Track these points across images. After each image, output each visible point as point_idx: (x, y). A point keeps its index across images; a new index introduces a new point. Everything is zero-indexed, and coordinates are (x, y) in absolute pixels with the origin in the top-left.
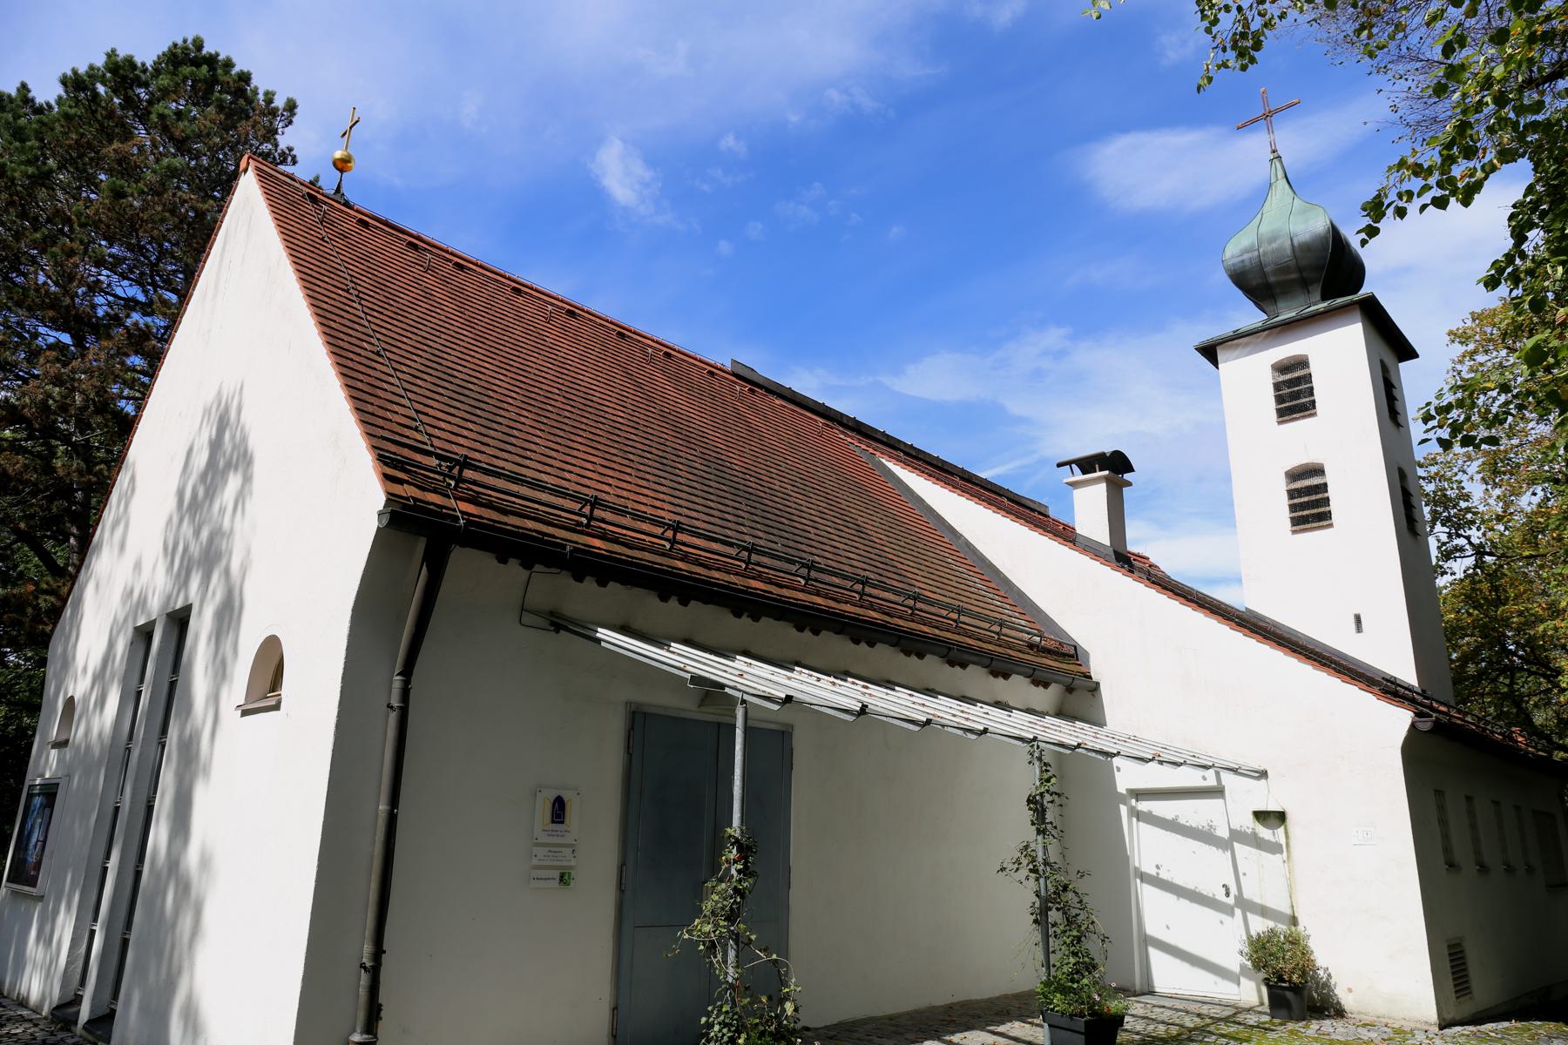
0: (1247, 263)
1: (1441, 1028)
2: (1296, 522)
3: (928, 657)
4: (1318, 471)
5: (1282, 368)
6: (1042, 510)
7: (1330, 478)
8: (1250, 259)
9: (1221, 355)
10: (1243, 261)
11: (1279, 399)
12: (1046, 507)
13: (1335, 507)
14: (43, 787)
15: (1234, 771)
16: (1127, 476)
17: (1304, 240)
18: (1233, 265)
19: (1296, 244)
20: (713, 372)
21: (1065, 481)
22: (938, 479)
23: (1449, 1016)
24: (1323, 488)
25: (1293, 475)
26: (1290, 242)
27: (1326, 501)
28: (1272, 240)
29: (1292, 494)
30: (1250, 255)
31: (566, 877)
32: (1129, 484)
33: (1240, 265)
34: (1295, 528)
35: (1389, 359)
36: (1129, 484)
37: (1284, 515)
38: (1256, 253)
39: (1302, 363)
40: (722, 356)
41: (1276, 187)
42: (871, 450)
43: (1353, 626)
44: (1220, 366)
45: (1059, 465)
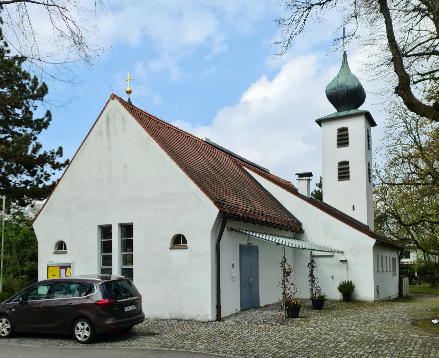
0: (333, 93)
3: (264, 226)
4: (347, 163)
5: (340, 130)
6: (268, 171)
7: (351, 166)
8: (334, 92)
10: (332, 93)
11: (338, 140)
12: (269, 170)
13: (351, 174)
14: (126, 271)
16: (311, 178)
18: (329, 93)
19: (348, 90)
23: (131, 264)
24: (348, 168)
25: (341, 164)
26: (347, 89)
27: (349, 173)
28: (342, 87)
29: (339, 170)
31: (6, 253)
32: (311, 180)
35: (368, 126)
36: (311, 180)
38: (336, 91)
39: (346, 129)
43: (352, 209)
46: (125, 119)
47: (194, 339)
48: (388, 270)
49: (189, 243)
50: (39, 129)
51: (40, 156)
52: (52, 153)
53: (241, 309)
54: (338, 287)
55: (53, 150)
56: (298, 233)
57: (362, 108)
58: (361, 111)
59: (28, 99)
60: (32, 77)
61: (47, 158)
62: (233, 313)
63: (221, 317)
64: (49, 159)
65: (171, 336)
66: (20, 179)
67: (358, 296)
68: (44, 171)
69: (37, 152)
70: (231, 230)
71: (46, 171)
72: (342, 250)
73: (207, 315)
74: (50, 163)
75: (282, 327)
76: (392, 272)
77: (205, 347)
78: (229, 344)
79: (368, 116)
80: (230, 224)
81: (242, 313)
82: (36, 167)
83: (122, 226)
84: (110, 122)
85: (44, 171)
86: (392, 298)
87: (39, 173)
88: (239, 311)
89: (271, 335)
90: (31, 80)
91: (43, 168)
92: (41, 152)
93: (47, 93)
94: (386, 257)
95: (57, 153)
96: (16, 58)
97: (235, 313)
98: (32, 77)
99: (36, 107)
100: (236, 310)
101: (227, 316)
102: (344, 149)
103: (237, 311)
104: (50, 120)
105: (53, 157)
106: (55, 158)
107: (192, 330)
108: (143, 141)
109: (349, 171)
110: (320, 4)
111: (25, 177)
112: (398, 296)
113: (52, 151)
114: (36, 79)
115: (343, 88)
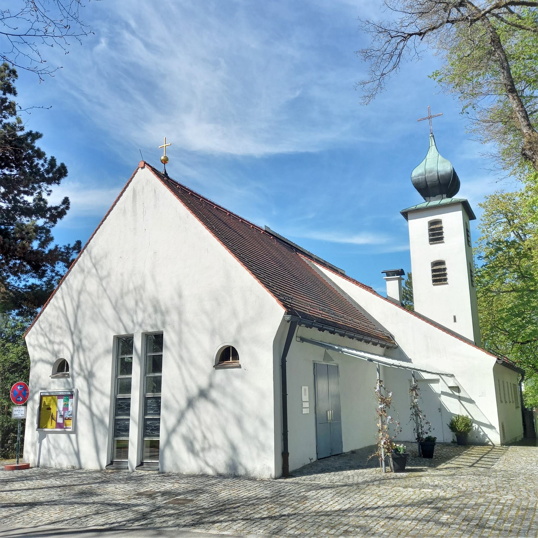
0: (420, 180)
1: (501, 445)
2: (434, 281)
4: (442, 263)
5: (432, 223)
6: (343, 272)
7: (447, 266)
8: (422, 178)
9: (409, 216)
10: (419, 179)
15: (447, 375)
17: (442, 174)
19: (439, 175)
20: (258, 229)
21: (384, 278)
22: (324, 266)
24: (445, 269)
28: (430, 172)
29: (433, 271)
30: (422, 177)
33: (418, 180)
34: (434, 283)
35: (467, 218)
37: (430, 279)
38: (424, 176)
39: (439, 222)
40: (261, 223)
41: (431, 148)
42: (310, 260)
44: (409, 221)
45: (382, 273)
46: (157, 193)
47: (248, 511)
48: (508, 401)
49: (243, 359)
50: (53, 219)
51: (50, 251)
52: (67, 248)
53: (317, 456)
54: (449, 424)
55: (69, 245)
56: (390, 349)
57: (458, 197)
58: (456, 200)
59: (42, 183)
60: (49, 157)
61: (60, 255)
62: (306, 464)
63: (289, 471)
64: (63, 256)
65: (212, 504)
66: (23, 283)
67: (477, 437)
68: (56, 271)
69: (47, 246)
70: (303, 340)
71: (58, 272)
72: (451, 373)
73: (269, 469)
74: (63, 260)
75: (384, 487)
76: (514, 403)
77: (267, 527)
78: (305, 521)
79: (465, 206)
80: (301, 330)
81: (319, 463)
82: (44, 266)
83: (146, 336)
84: (138, 197)
85: (56, 271)
86: (518, 440)
87: (49, 273)
88: (315, 460)
89: (370, 502)
90: (47, 162)
91: (54, 267)
92: (51, 246)
93: (66, 176)
94: (507, 382)
95: (74, 248)
96: (30, 134)
97: (309, 464)
98: (48, 157)
99: (51, 191)
100: (311, 460)
101: (298, 469)
102: (438, 247)
103: (312, 461)
104: (67, 208)
105: (68, 253)
106: (71, 255)
107: (246, 494)
108: (180, 219)
109: (445, 272)
110: (420, 34)
111: (33, 281)
112: (522, 436)
113: (67, 246)
114: (53, 160)
115: (433, 173)
